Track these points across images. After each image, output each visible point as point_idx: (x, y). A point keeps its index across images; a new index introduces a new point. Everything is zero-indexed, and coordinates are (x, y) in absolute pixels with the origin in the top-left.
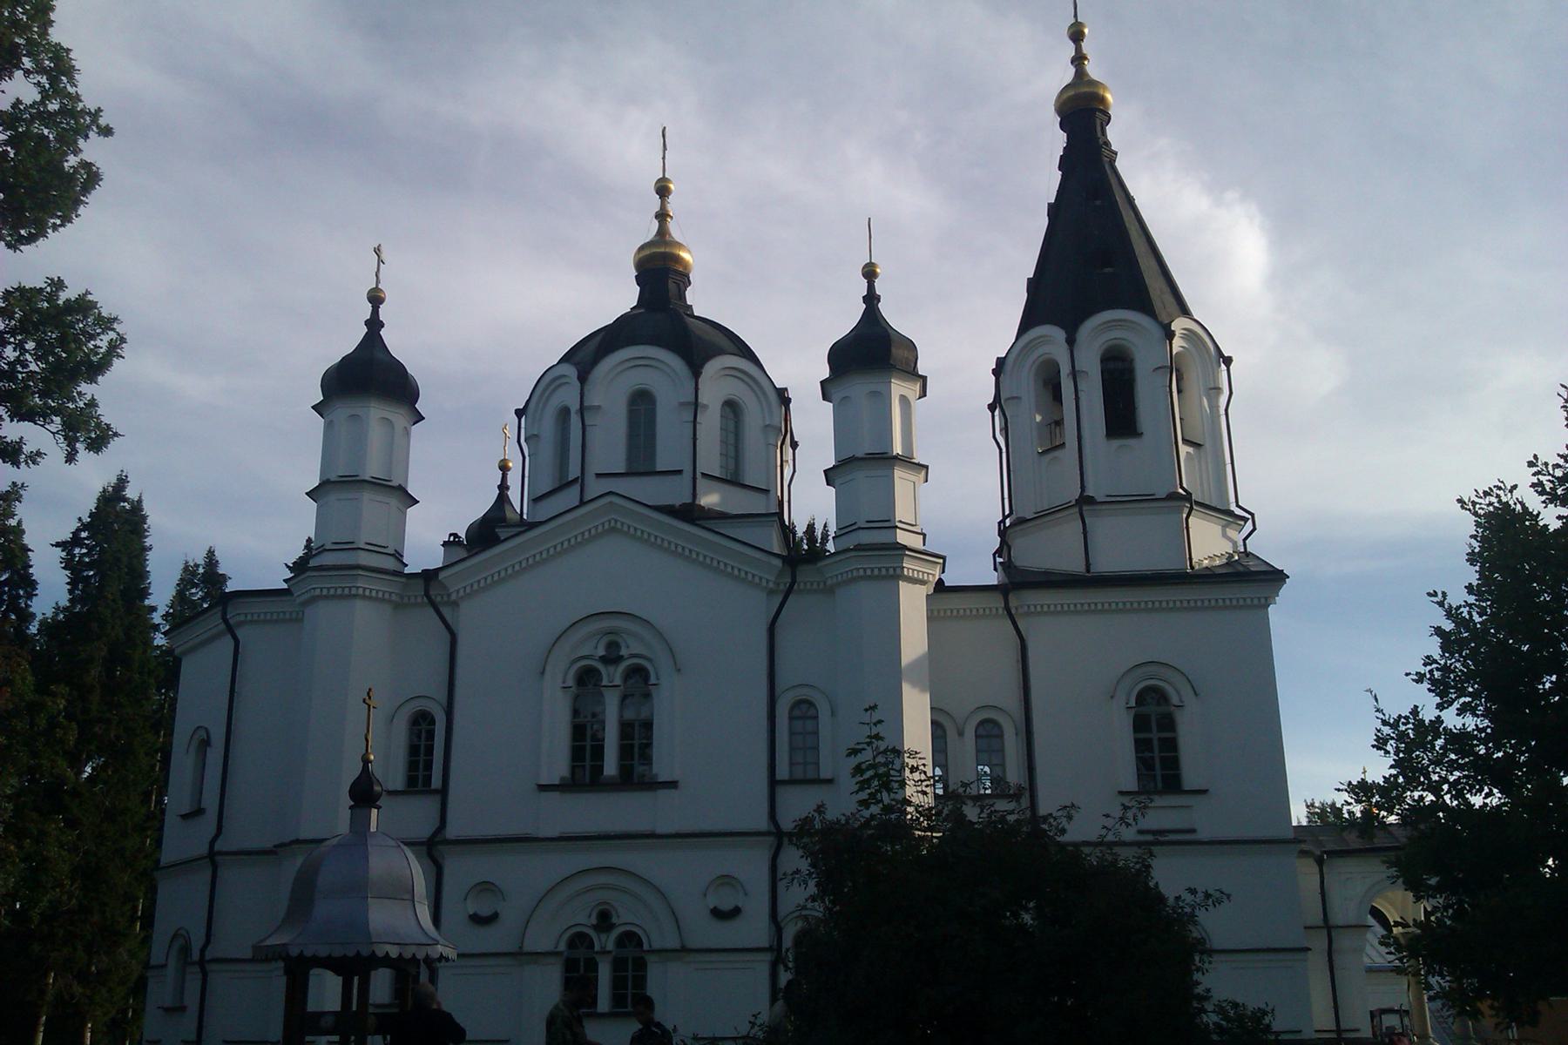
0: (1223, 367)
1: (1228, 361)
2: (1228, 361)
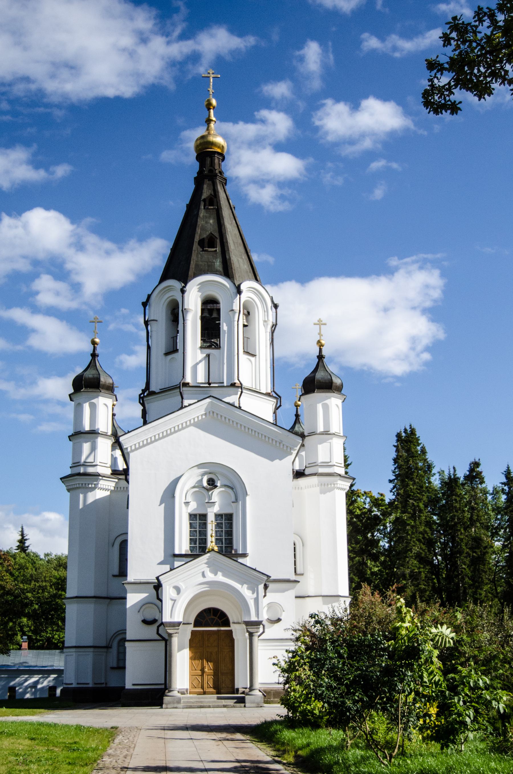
1: (276, 306)
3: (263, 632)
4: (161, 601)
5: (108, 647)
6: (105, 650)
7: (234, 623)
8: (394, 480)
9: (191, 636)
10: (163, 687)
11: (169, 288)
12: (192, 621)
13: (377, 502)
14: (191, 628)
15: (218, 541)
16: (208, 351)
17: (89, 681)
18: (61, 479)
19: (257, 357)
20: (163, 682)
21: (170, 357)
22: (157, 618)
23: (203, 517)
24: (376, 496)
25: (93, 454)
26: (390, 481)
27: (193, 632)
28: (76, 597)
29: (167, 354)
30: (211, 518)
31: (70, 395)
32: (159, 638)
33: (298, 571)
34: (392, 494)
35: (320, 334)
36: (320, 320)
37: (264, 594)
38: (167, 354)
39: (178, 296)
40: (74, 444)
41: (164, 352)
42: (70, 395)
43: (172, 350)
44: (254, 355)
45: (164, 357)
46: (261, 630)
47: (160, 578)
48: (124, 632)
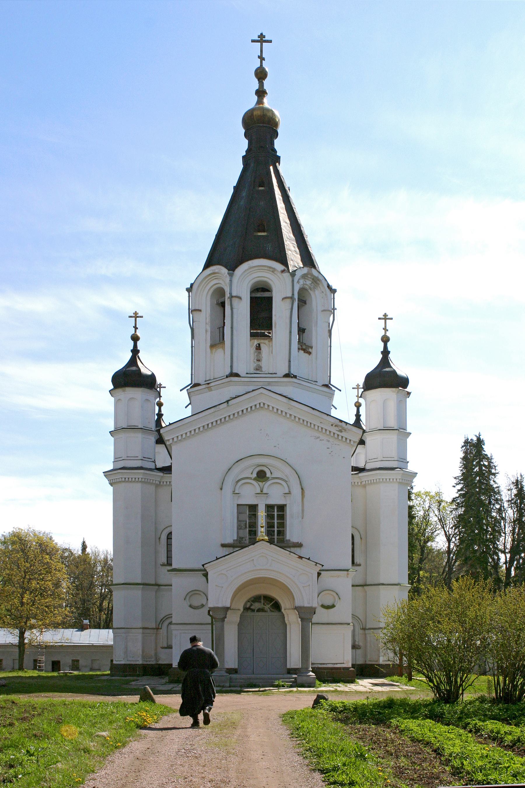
15: (269, 533)
16: (256, 342)
23: (253, 508)
25: (231, 550)
35: (385, 329)
48: (169, 616)
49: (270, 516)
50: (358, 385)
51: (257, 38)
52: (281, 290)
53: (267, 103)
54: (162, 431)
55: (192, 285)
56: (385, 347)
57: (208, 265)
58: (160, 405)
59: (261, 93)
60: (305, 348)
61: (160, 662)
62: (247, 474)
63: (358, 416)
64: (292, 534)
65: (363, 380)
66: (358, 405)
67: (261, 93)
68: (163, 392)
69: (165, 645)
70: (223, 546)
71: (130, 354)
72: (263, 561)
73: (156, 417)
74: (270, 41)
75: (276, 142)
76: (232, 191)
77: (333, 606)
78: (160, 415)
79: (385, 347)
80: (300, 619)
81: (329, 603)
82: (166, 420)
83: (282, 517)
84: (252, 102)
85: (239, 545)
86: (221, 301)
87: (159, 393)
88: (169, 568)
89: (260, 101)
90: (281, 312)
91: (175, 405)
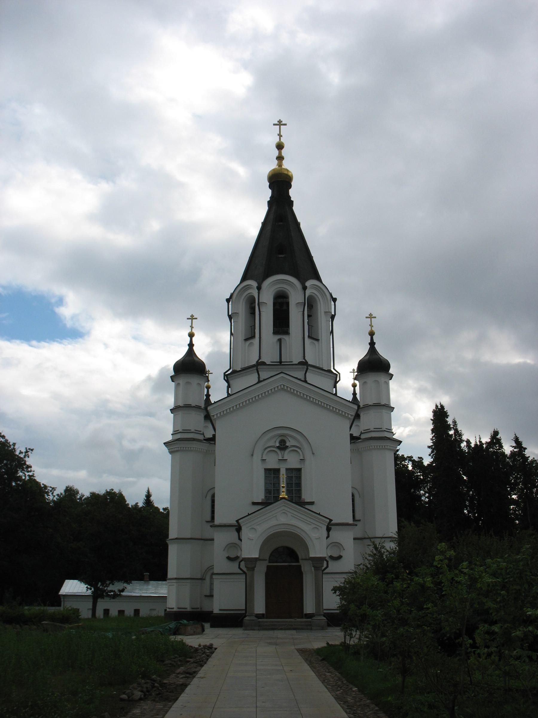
0: (333, 303)
1: (335, 300)
2: (335, 300)
3: (327, 567)
4: (241, 540)
5: (202, 579)
6: (200, 581)
7: (302, 559)
8: (432, 446)
9: (267, 569)
10: (244, 612)
11: (248, 287)
12: (267, 556)
13: (417, 464)
14: (266, 563)
15: (289, 492)
16: (279, 337)
17: (187, 606)
18: (164, 443)
19: (320, 341)
20: (244, 608)
21: (248, 343)
22: (239, 555)
23: (277, 471)
24: (417, 459)
25: (260, 507)
26: (429, 447)
27: (268, 567)
28: (176, 539)
29: (246, 340)
30: (283, 472)
31: (171, 377)
32: (241, 572)
33: (357, 518)
34: (430, 457)
35: (371, 326)
36: (371, 315)
37: (326, 535)
38: (246, 340)
39: (255, 293)
40: (174, 416)
41: (244, 338)
42: (171, 377)
43: (250, 336)
44: (317, 340)
45: (243, 342)
46: (325, 565)
47: (240, 521)
48: (211, 567)
49: (289, 478)
50: (354, 370)
51: (277, 123)
52: (295, 298)
53: (286, 165)
54: (209, 408)
55: (232, 295)
56: (372, 339)
57: (244, 278)
58: (208, 388)
59: (280, 158)
60: (314, 338)
61: (215, 580)
62: (271, 443)
63: (354, 394)
64: (306, 496)
65: (357, 366)
66: (354, 386)
67: (280, 158)
68: (211, 377)
69: (208, 594)
70: (254, 504)
71: (187, 348)
72: (283, 517)
73: (205, 397)
74: (285, 125)
75: (290, 190)
76: (260, 225)
77: (340, 557)
78: (208, 396)
79: (372, 339)
80: (313, 568)
81: (335, 555)
82: (213, 399)
83: (299, 478)
84: (273, 165)
85: (265, 504)
86: (252, 306)
87: (208, 377)
88: (212, 524)
89: (280, 165)
90: (296, 317)
91: (218, 391)
